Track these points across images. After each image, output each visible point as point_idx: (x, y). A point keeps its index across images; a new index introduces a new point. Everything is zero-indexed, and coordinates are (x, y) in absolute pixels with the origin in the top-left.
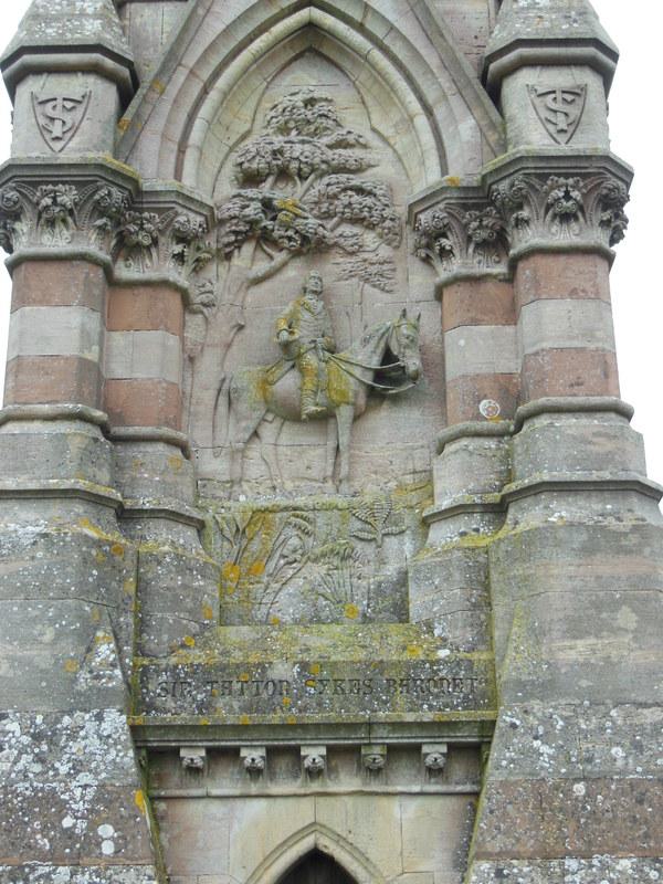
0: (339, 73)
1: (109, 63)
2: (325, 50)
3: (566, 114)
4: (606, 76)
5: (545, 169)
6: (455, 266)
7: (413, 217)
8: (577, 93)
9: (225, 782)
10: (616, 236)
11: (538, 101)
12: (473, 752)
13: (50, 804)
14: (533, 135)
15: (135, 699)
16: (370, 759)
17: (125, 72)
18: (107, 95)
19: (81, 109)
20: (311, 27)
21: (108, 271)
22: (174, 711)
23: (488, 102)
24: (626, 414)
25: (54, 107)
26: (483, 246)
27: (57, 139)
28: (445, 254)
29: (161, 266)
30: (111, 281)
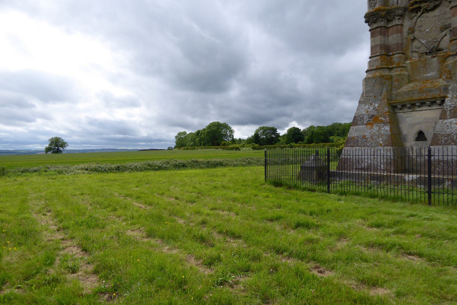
27: (373, 7)
29: (397, 22)
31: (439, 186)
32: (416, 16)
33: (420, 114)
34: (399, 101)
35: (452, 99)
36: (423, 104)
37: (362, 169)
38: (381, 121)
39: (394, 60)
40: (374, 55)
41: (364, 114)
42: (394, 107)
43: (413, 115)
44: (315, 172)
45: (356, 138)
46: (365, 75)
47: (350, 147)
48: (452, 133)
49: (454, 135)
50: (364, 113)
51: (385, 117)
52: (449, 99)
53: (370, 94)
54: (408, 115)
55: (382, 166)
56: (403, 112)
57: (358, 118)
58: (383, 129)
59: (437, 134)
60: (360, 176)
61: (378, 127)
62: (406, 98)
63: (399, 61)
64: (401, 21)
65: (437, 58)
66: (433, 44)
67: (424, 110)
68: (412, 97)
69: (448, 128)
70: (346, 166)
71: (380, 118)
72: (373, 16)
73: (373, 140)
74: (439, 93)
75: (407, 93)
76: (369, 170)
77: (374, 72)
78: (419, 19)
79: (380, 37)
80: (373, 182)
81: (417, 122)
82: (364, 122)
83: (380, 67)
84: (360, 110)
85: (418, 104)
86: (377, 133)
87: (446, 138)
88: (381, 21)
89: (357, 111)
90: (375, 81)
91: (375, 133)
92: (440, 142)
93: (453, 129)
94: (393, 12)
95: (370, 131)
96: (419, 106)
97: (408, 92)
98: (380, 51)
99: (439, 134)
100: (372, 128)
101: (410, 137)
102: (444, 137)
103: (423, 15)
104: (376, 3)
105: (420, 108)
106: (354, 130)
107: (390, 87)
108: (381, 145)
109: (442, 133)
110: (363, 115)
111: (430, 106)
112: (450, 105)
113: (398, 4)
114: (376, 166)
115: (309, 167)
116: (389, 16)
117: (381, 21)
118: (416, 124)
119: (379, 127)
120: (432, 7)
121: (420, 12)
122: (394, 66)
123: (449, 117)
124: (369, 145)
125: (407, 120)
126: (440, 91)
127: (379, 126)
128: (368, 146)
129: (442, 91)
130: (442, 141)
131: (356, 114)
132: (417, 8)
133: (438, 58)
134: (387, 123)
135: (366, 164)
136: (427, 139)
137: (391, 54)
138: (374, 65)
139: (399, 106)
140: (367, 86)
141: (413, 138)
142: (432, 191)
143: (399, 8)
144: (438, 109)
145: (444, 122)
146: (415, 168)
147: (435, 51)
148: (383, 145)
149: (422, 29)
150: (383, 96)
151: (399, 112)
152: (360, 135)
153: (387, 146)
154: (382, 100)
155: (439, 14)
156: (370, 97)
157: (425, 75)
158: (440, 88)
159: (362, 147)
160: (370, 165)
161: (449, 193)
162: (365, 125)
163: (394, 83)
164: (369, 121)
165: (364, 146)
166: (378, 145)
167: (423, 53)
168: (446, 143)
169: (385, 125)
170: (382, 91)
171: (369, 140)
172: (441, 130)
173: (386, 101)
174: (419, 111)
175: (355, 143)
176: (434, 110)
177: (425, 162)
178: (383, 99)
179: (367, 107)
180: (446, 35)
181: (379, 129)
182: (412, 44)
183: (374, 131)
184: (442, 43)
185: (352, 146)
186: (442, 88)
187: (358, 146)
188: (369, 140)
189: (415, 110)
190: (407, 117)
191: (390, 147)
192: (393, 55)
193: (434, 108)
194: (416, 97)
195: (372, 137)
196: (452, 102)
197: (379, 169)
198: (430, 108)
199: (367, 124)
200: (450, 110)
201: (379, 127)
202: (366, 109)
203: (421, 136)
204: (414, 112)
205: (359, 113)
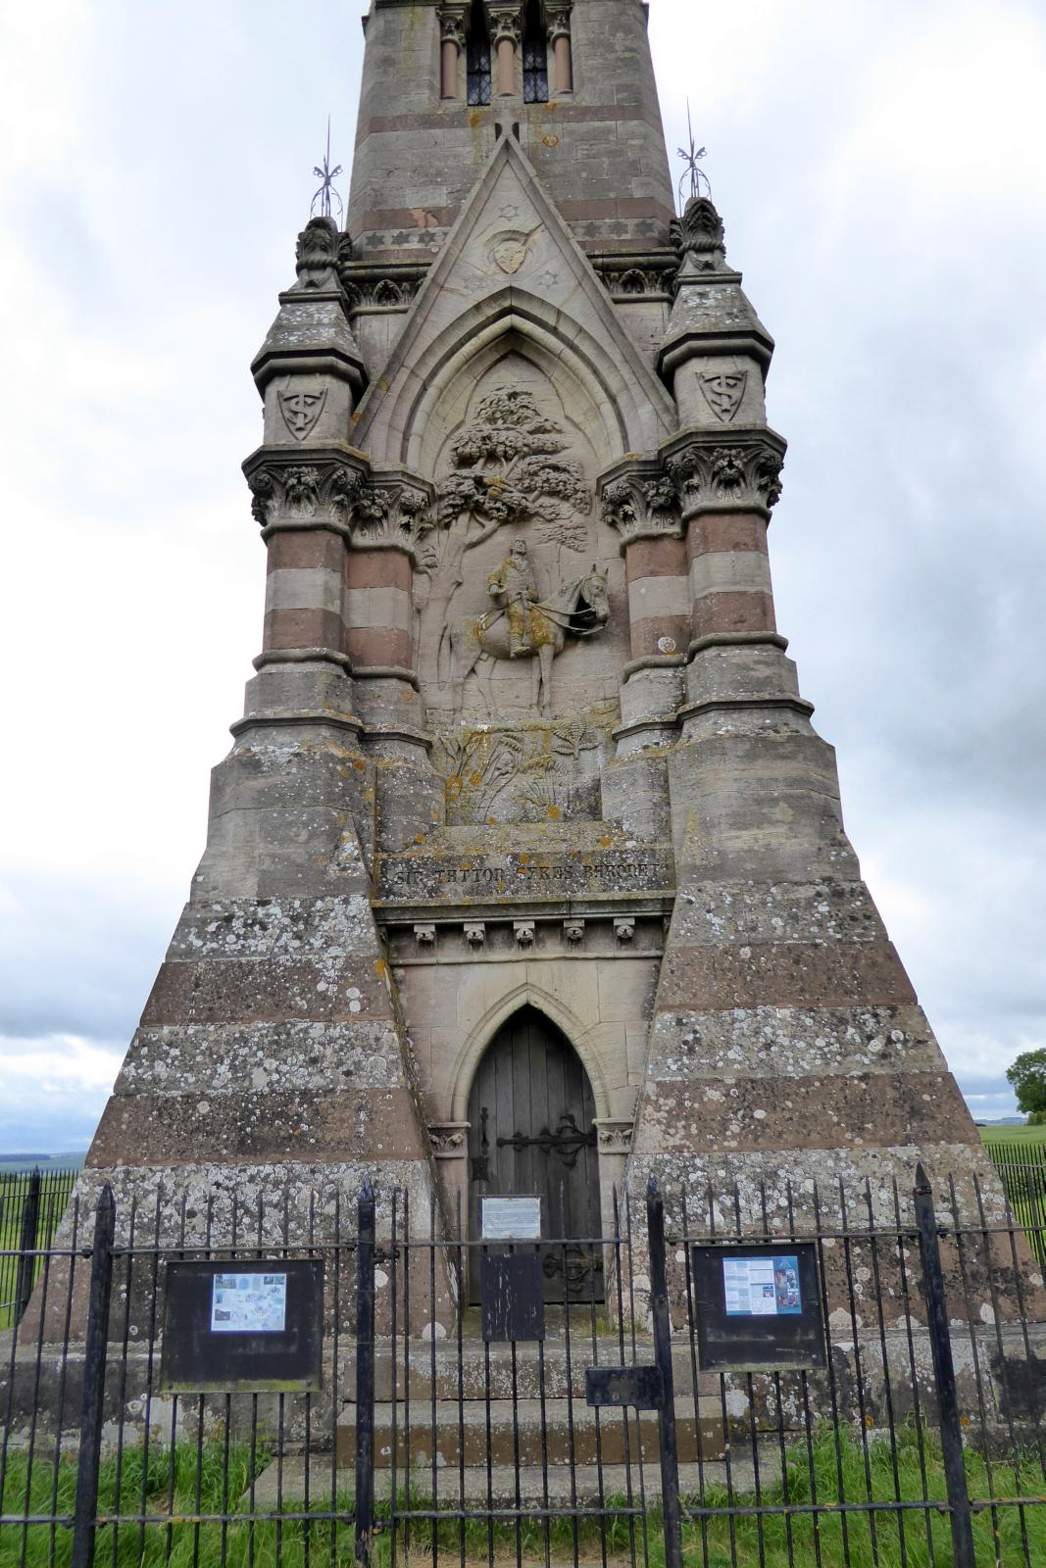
1: (342, 365)
3: (729, 397)
4: (764, 363)
5: (710, 442)
6: (637, 528)
7: (601, 488)
12: (655, 924)
13: (307, 973)
14: (700, 412)
15: (376, 886)
16: (570, 931)
17: (356, 372)
18: (341, 392)
19: (319, 403)
20: (512, 332)
21: (347, 538)
22: (411, 895)
24: (806, 710)
28: (628, 518)
29: (390, 533)
30: (351, 549)
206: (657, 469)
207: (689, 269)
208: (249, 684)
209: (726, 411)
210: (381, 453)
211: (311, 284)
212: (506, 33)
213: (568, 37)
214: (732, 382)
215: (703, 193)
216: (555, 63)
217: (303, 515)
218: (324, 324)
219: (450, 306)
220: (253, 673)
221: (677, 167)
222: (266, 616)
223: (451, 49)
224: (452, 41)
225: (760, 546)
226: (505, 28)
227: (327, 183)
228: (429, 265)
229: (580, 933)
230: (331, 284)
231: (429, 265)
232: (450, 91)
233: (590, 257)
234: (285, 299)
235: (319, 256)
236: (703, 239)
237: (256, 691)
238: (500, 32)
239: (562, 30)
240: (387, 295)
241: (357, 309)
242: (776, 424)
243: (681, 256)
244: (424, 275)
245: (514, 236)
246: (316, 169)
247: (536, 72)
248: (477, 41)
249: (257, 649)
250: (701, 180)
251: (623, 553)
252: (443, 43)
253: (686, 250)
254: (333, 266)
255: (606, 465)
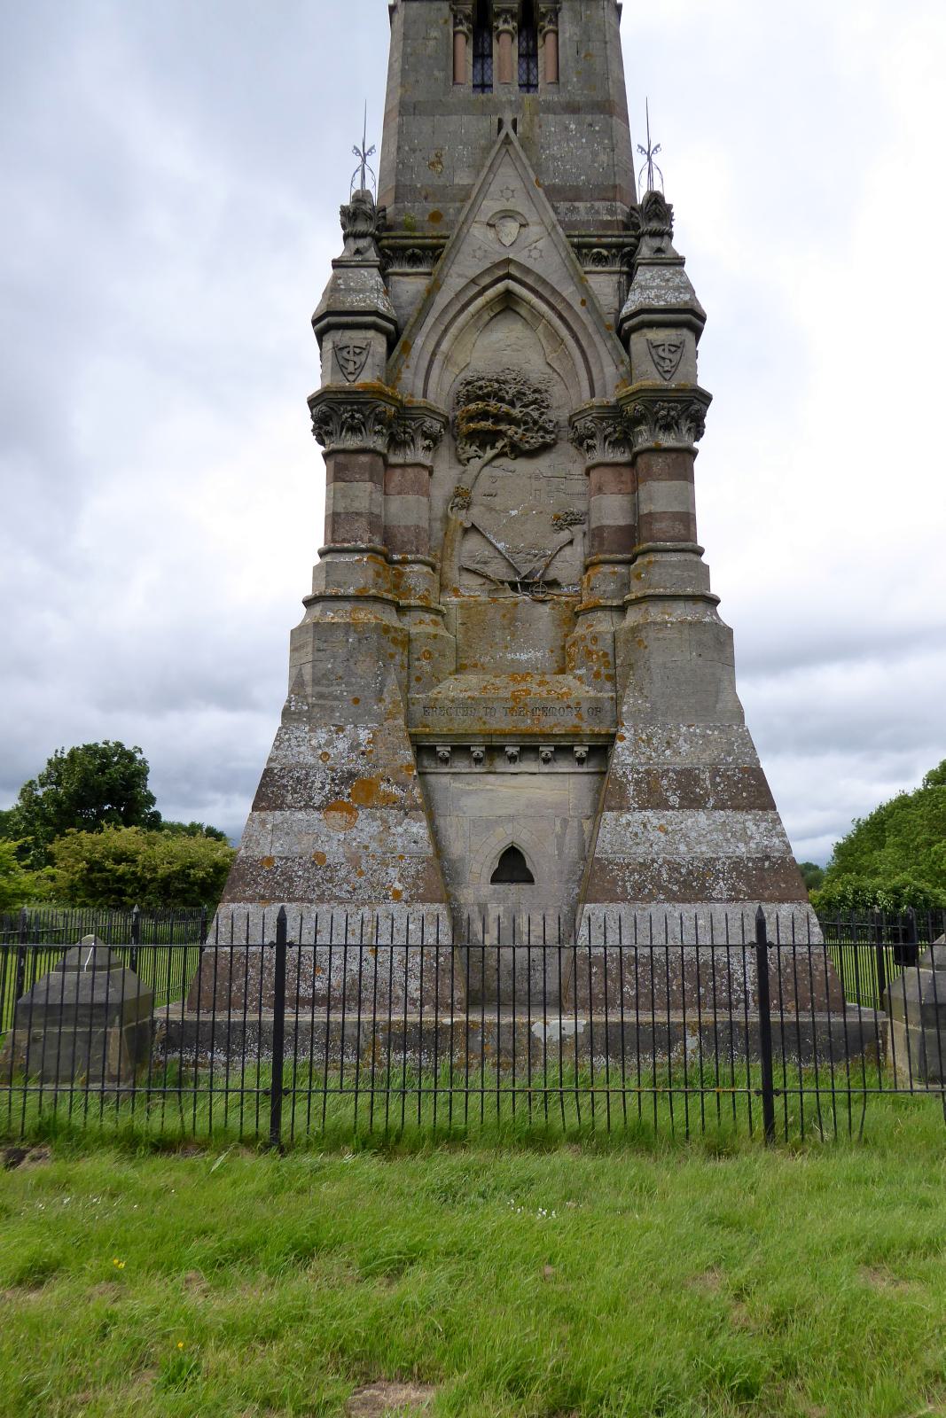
0: (514, 315)
1: (379, 321)
2: (518, 310)
3: (671, 361)
4: (697, 332)
5: (653, 397)
6: (598, 456)
7: (571, 424)
8: (677, 347)
9: (461, 765)
10: (699, 434)
11: (653, 351)
14: (649, 376)
16: (441, 754)
17: (391, 327)
18: (379, 344)
19: (365, 353)
20: (508, 293)
21: (384, 457)
23: (623, 351)
24: (714, 601)
25: (349, 352)
26: (615, 444)
27: (351, 373)
28: (590, 448)
29: (417, 454)
30: (388, 466)
31: (405, 1053)
32: (480, 457)
33: (514, 787)
34: (450, 730)
35: (635, 743)
36: (529, 749)
37: (314, 1002)
38: (390, 802)
39: (412, 582)
40: (346, 545)
41: (311, 767)
42: (423, 749)
43: (488, 787)
44: (114, 1031)
45: (277, 863)
46: (298, 615)
47: (251, 900)
48: (653, 861)
49: (661, 866)
50: (311, 760)
51: (403, 785)
52: (626, 743)
53: (337, 690)
54: (468, 784)
55: (414, 985)
56: (453, 773)
57: (283, 777)
58: (400, 830)
59: (607, 859)
60: (336, 1035)
61: (379, 822)
62: (463, 723)
63: (427, 590)
64: (430, 455)
65: (549, 605)
66: (530, 561)
67: (526, 773)
68: (485, 723)
69: (638, 841)
70: (239, 990)
71: (384, 786)
72: (352, 404)
73: (361, 874)
74: (576, 721)
75: (467, 706)
76: (566, 1005)
77: (348, 606)
78: (487, 469)
79: (369, 485)
80: (400, 1057)
81: (499, 813)
82: (311, 798)
83: (373, 592)
84: (290, 746)
85: (511, 750)
86: (373, 846)
87: (637, 877)
88: (376, 433)
89: (277, 748)
90: (359, 641)
91: (366, 847)
92: (619, 890)
93: (655, 847)
94: (413, 419)
95: (342, 837)
96: (512, 759)
97: (469, 701)
98: (366, 538)
99: (610, 863)
100: (350, 825)
101: (476, 868)
102: (632, 873)
103: (497, 463)
104: (362, 366)
105: (512, 765)
106: (269, 826)
107: (404, 674)
108: (397, 894)
109: (619, 858)
110: (309, 768)
111: (546, 761)
112: (632, 765)
113: (425, 395)
114: (383, 987)
115: (77, 1005)
116: (401, 426)
117: (376, 433)
118: (500, 820)
119: (384, 821)
120: (536, 446)
121: (493, 447)
122: (413, 602)
123: (636, 806)
124: (344, 895)
125: (466, 802)
126: (579, 716)
127: (381, 818)
128: (341, 901)
129: (585, 716)
130: (624, 887)
131: (271, 760)
132: (488, 432)
133: (554, 609)
134: (415, 808)
135: (336, 980)
136: (535, 879)
137: (396, 557)
138: (345, 583)
139: (443, 751)
140: (321, 654)
141: (485, 870)
142: (776, 1087)
143: (434, 412)
144: (571, 776)
145: (623, 821)
146: (506, 985)
147: (535, 585)
148: (405, 895)
149: (497, 502)
150: (388, 703)
151: (436, 770)
152: (297, 849)
153: (423, 899)
154: (386, 719)
155: (550, 475)
156: (336, 698)
157: (510, 656)
158: (578, 703)
159: (311, 901)
160: (353, 980)
161: (788, 1088)
162: (318, 809)
163: (417, 663)
164: (338, 794)
165: (321, 899)
166: (386, 897)
167: (502, 582)
168: (640, 894)
169: (406, 814)
170: (383, 684)
171: (342, 873)
172: (615, 848)
173: (401, 722)
174: (509, 777)
175: (277, 883)
176: (560, 777)
177: (578, 962)
178: (391, 715)
179: (322, 736)
180: (571, 542)
181: (380, 833)
182: (461, 545)
183: (364, 837)
184: (557, 563)
185: (262, 897)
186: (585, 706)
187: (290, 900)
188: (342, 873)
189: (498, 770)
190: (469, 793)
191: (437, 905)
192: (404, 562)
193: (560, 770)
194: (501, 722)
195: (354, 861)
196: (638, 756)
197: (398, 998)
198: (546, 769)
199: (325, 807)
200: (637, 782)
201: (384, 821)
202: (320, 747)
203: (512, 867)
204: (491, 778)
205: (286, 756)
206: (614, 413)
207: (645, 251)
208: (316, 569)
209: (668, 371)
210: (411, 384)
211: (358, 252)
212: (506, 27)
213: (556, 33)
214: (673, 349)
215: (657, 188)
216: (545, 52)
217: (352, 442)
218: (368, 290)
219: (462, 269)
220: (317, 560)
221: (639, 161)
222: (326, 517)
223: (461, 39)
224: (463, 33)
225: (688, 476)
226: (505, 21)
227: (364, 161)
228: (448, 237)
229: (447, 754)
230: (372, 255)
231: (448, 237)
232: (460, 78)
233: (568, 236)
234: (336, 264)
235: (361, 227)
236: (654, 225)
237: (324, 572)
238: (502, 27)
239: (551, 27)
240: (414, 260)
241: (390, 270)
242: (703, 383)
243: (638, 238)
244: (443, 246)
245: (508, 214)
246: (355, 148)
247: (529, 56)
248: (481, 28)
249: (321, 544)
250: (656, 172)
251: (588, 473)
252: (455, 33)
253: (643, 235)
254: (372, 235)
255: (578, 407)
